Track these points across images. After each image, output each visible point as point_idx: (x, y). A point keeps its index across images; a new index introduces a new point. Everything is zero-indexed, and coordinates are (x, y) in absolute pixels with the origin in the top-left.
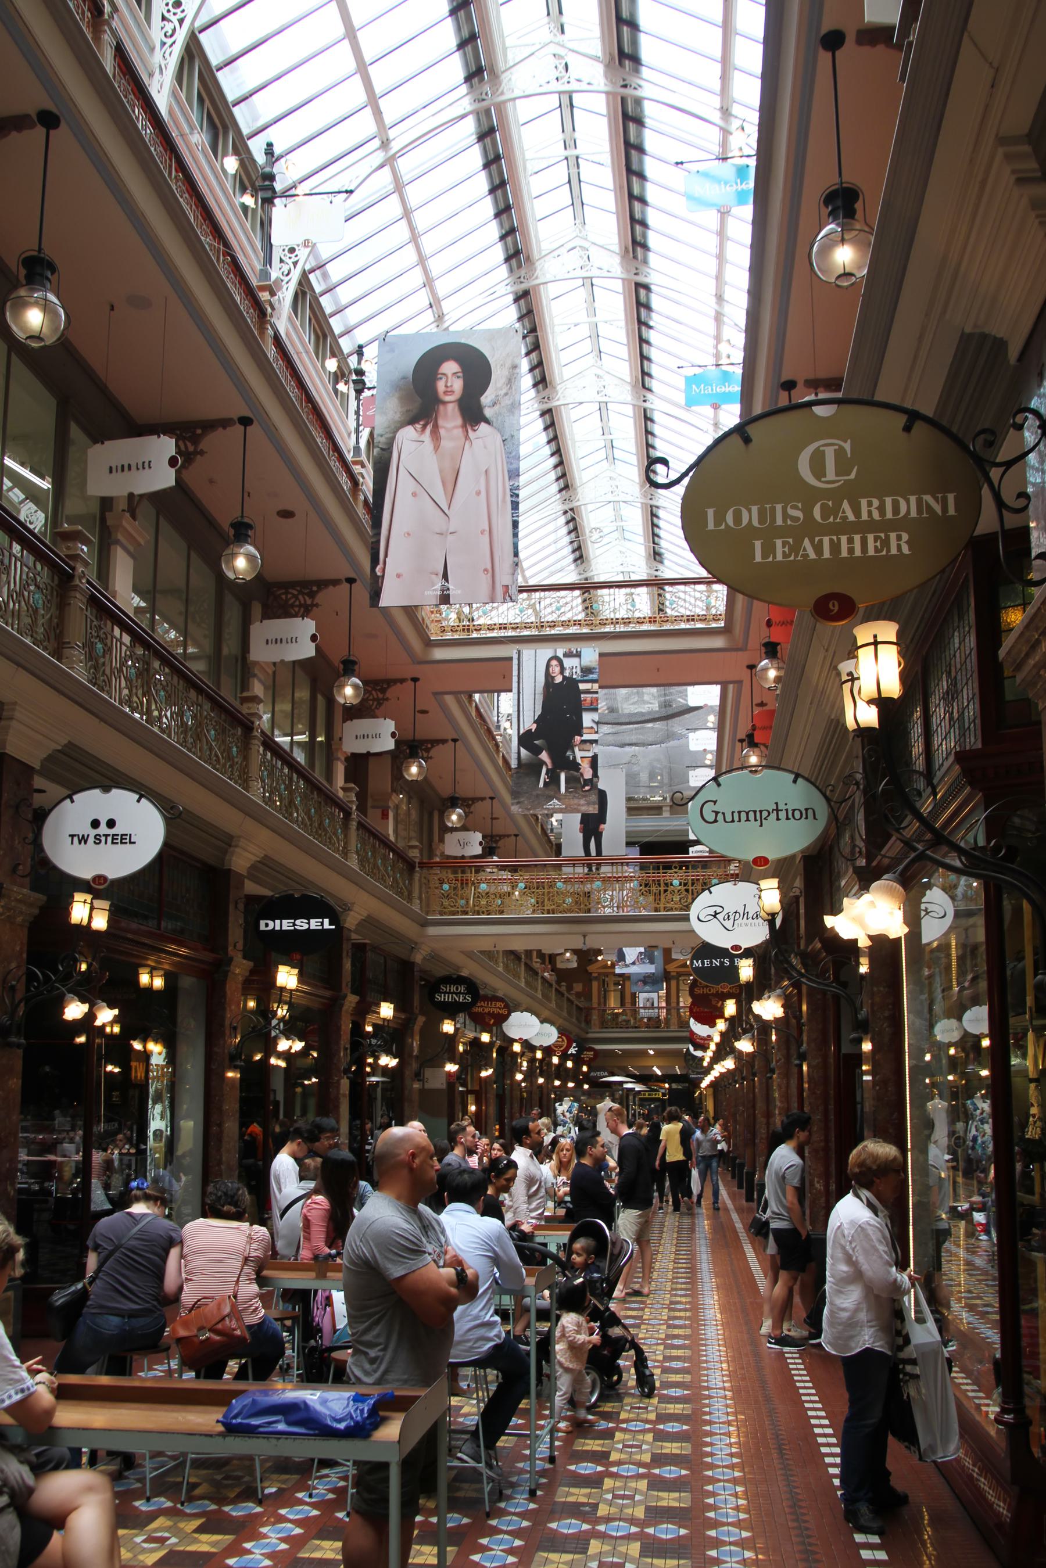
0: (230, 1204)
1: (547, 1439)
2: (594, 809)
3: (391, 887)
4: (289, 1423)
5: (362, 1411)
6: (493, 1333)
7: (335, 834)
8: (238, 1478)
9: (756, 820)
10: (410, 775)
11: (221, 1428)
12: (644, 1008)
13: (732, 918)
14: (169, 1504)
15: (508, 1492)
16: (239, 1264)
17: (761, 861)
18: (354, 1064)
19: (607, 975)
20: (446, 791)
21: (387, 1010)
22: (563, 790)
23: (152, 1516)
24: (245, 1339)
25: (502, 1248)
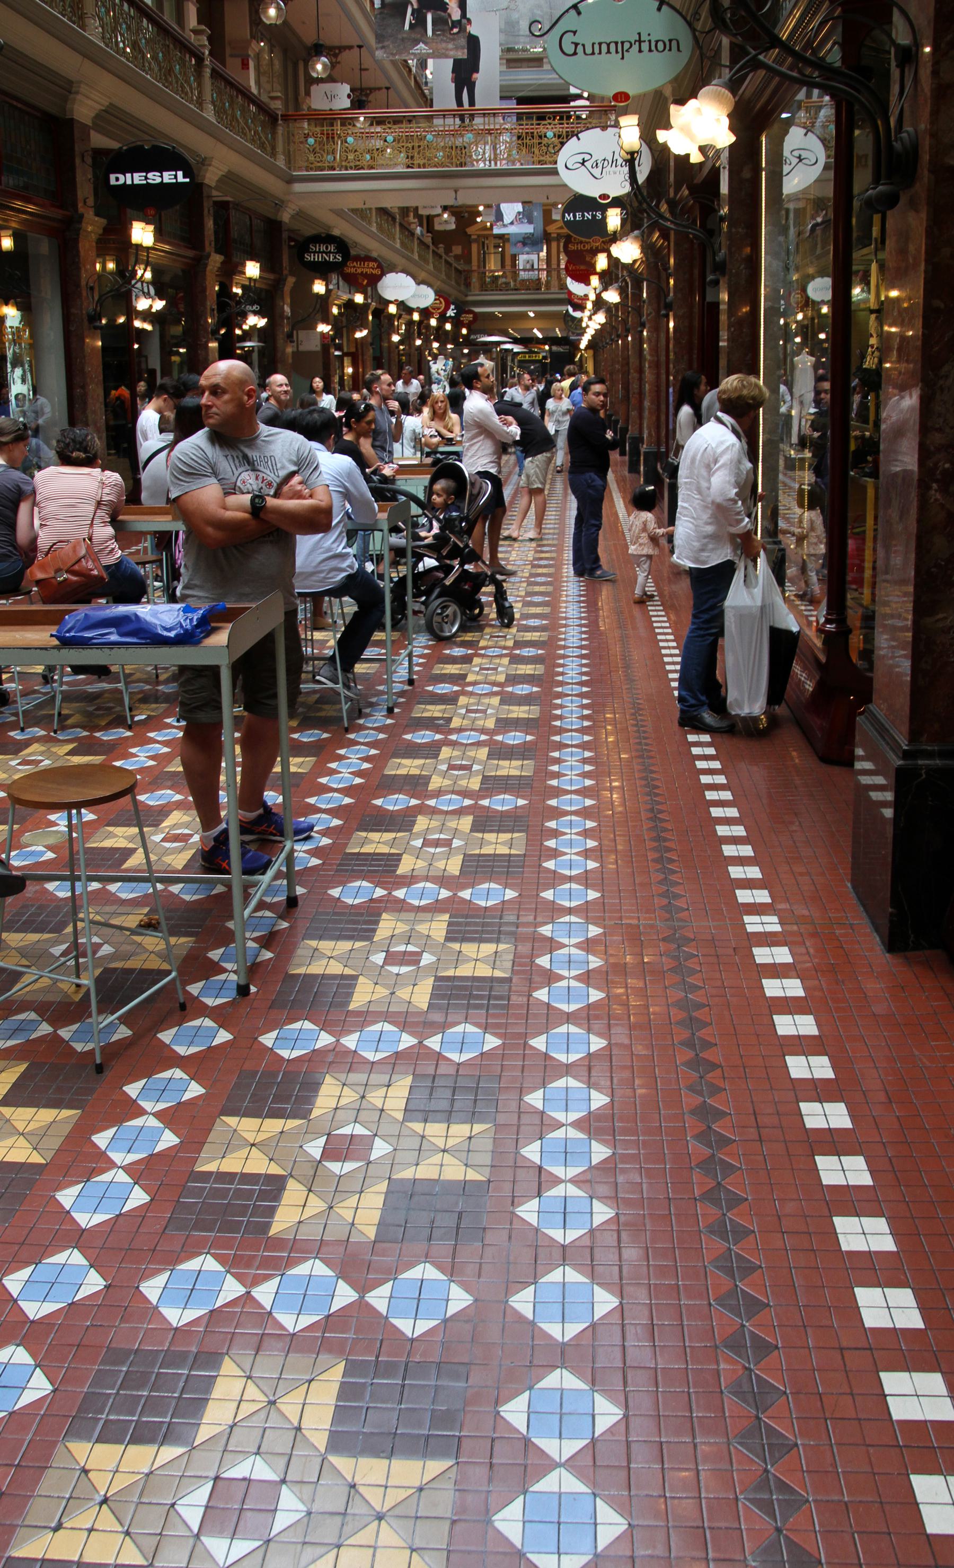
0: (79, 450)
1: (406, 664)
2: (463, 54)
3: (253, 141)
4: (121, 635)
5: (191, 620)
6: (345, 565)
7: (187, 82)
8: (110, 708)
9: (617, 52)
10: (269, 18)
11: (56, 642)
12: (524, 270)
13: (600, 165)
14: (43, 733)
15: (368, 710)
16: (92, 508)
17: (621, 96)
18: (223, 327)
19: (487, 237)
20: (309, 38)
21: (252, 269)
22: (430, 32)
23: (27, 743)
24: (102, 578)
25: (353, 484)
